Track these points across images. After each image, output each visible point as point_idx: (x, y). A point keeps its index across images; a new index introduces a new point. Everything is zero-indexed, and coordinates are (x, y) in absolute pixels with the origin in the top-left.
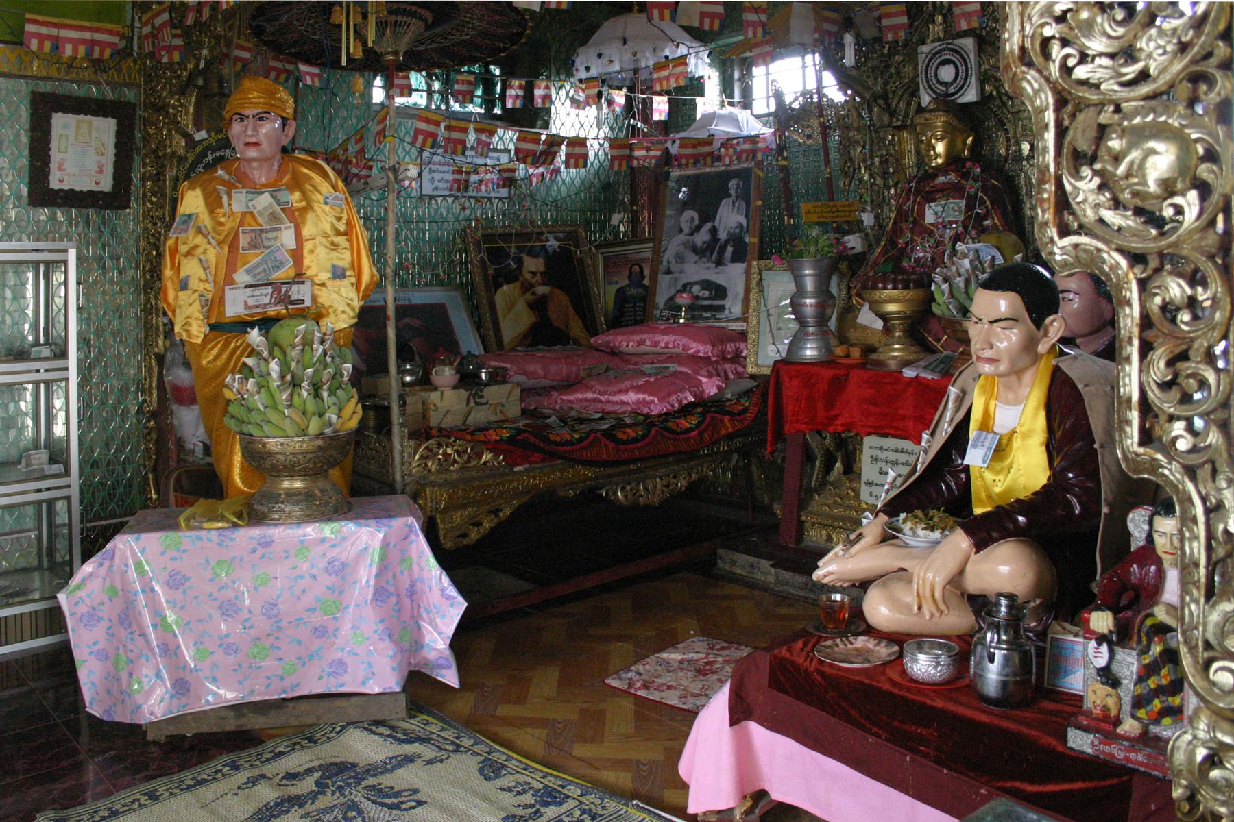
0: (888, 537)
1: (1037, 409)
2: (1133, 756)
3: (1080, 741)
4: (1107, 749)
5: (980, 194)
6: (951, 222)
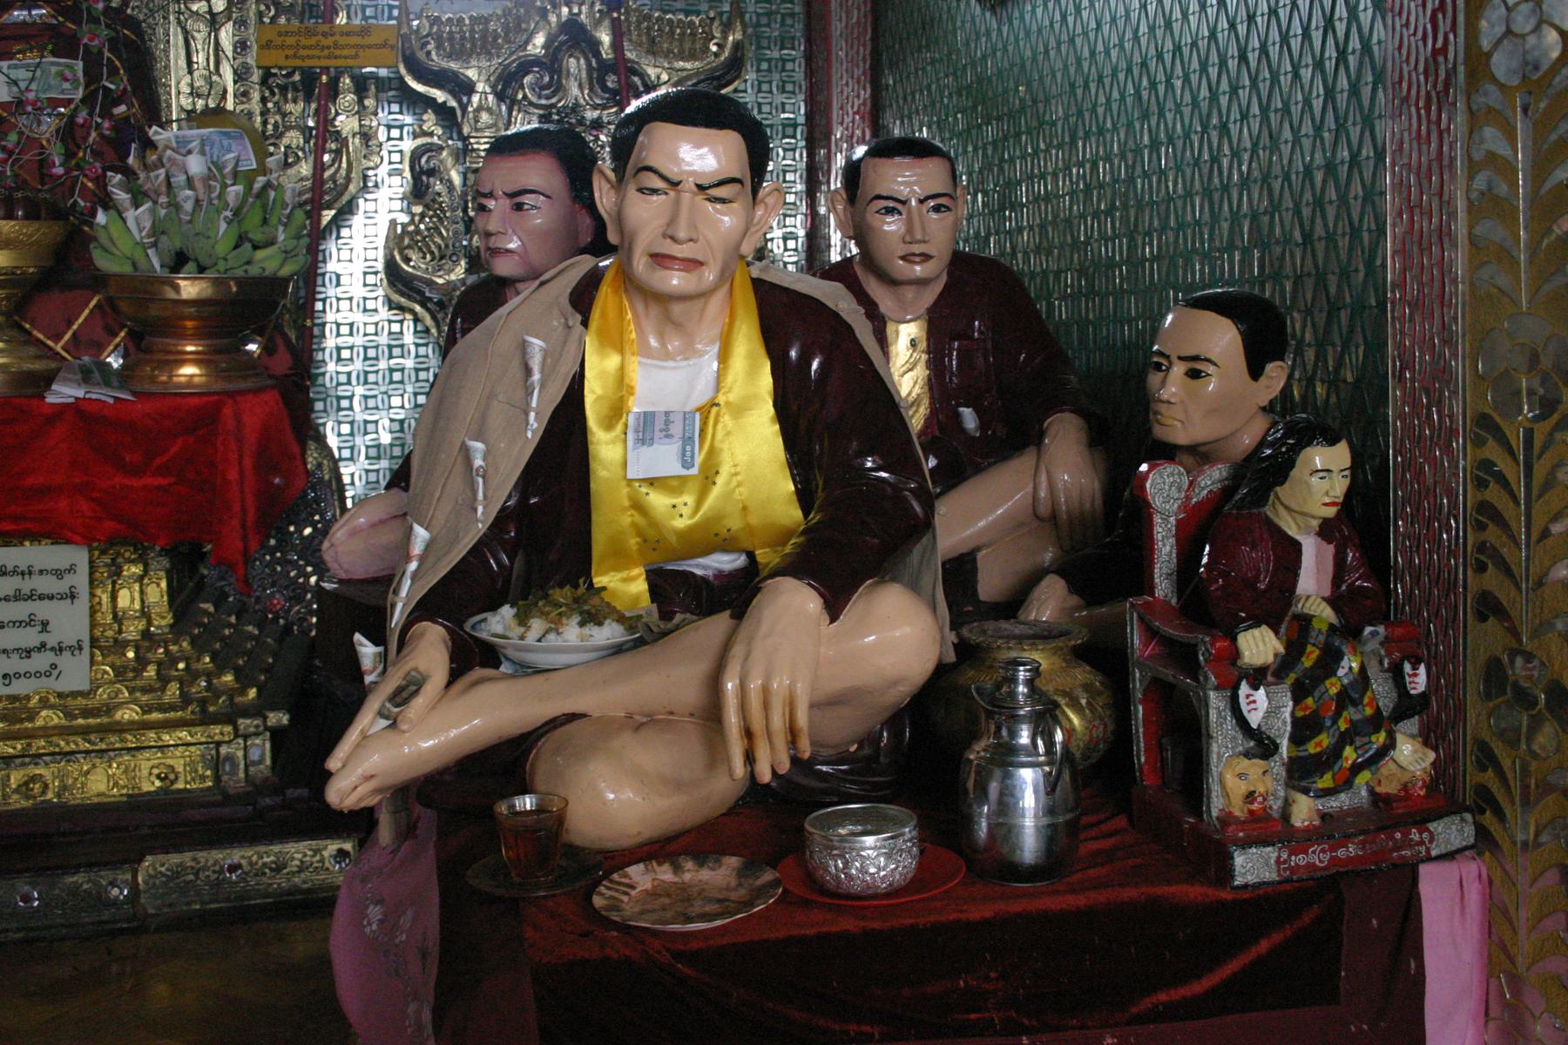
0: (472, 657)
1: (751, 356)
2: (1341, 853)
3: (1253, 866)
4: (1301, 860)
5: (107, 54)
6: (55, 103)
